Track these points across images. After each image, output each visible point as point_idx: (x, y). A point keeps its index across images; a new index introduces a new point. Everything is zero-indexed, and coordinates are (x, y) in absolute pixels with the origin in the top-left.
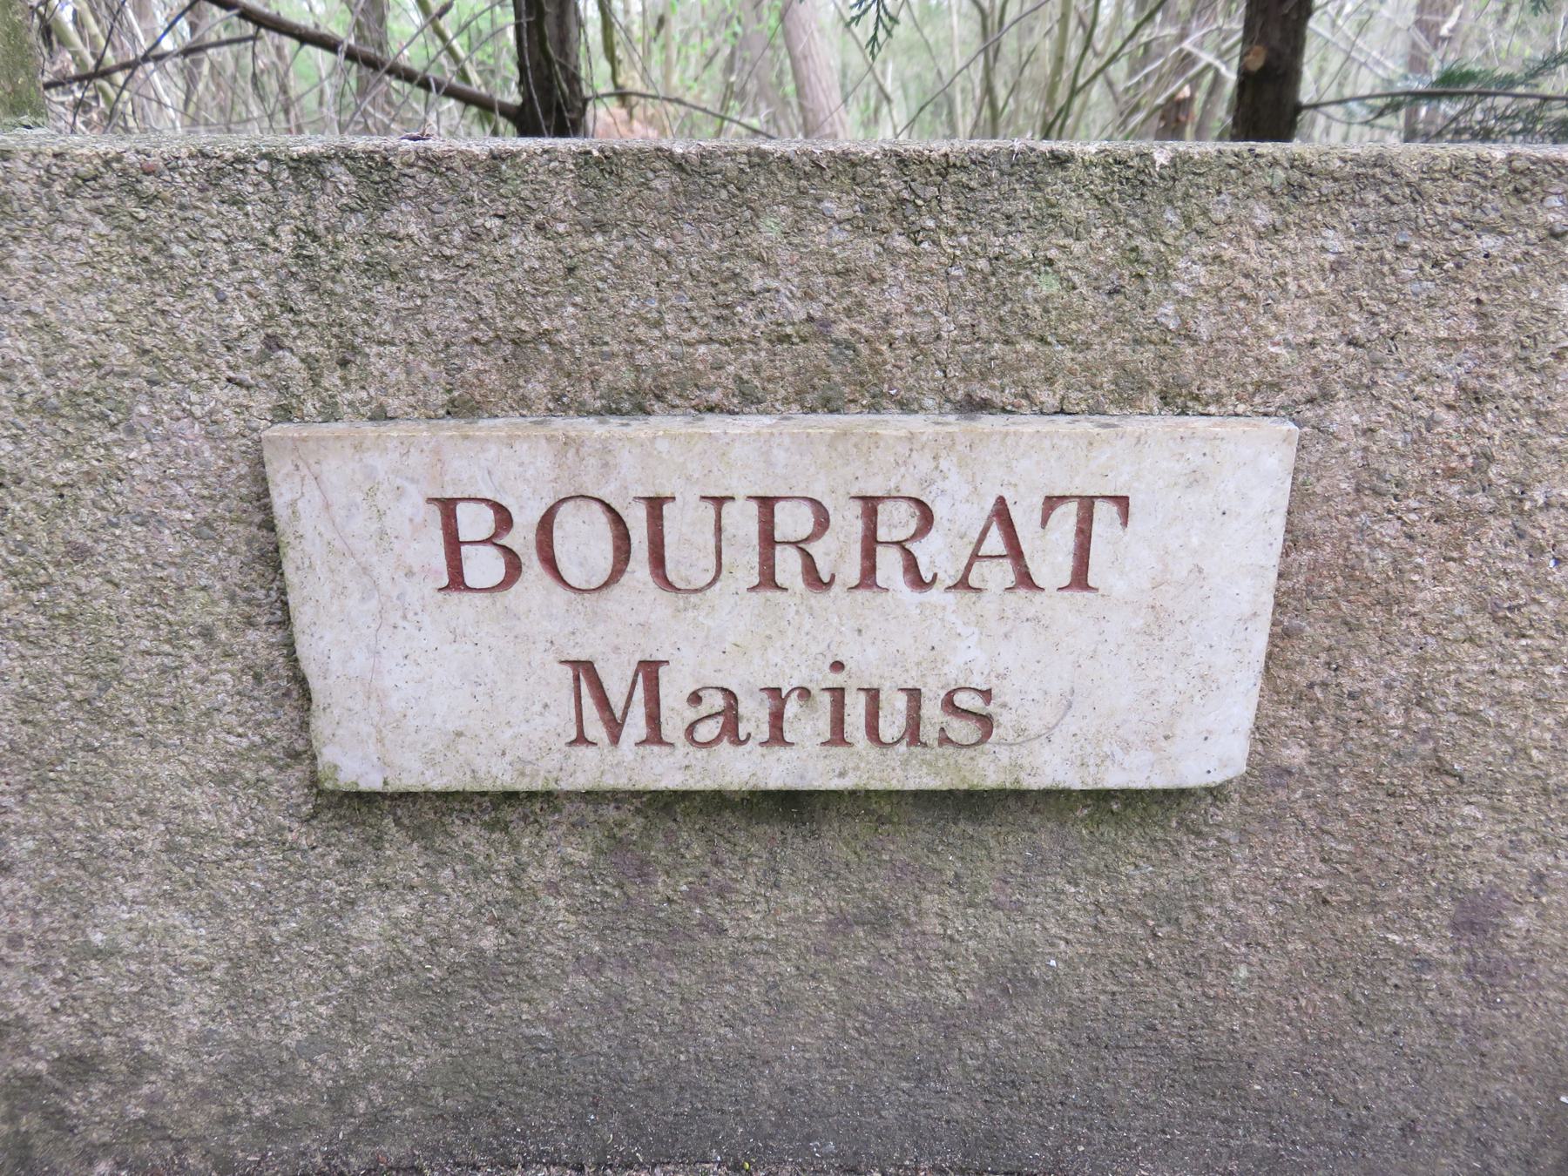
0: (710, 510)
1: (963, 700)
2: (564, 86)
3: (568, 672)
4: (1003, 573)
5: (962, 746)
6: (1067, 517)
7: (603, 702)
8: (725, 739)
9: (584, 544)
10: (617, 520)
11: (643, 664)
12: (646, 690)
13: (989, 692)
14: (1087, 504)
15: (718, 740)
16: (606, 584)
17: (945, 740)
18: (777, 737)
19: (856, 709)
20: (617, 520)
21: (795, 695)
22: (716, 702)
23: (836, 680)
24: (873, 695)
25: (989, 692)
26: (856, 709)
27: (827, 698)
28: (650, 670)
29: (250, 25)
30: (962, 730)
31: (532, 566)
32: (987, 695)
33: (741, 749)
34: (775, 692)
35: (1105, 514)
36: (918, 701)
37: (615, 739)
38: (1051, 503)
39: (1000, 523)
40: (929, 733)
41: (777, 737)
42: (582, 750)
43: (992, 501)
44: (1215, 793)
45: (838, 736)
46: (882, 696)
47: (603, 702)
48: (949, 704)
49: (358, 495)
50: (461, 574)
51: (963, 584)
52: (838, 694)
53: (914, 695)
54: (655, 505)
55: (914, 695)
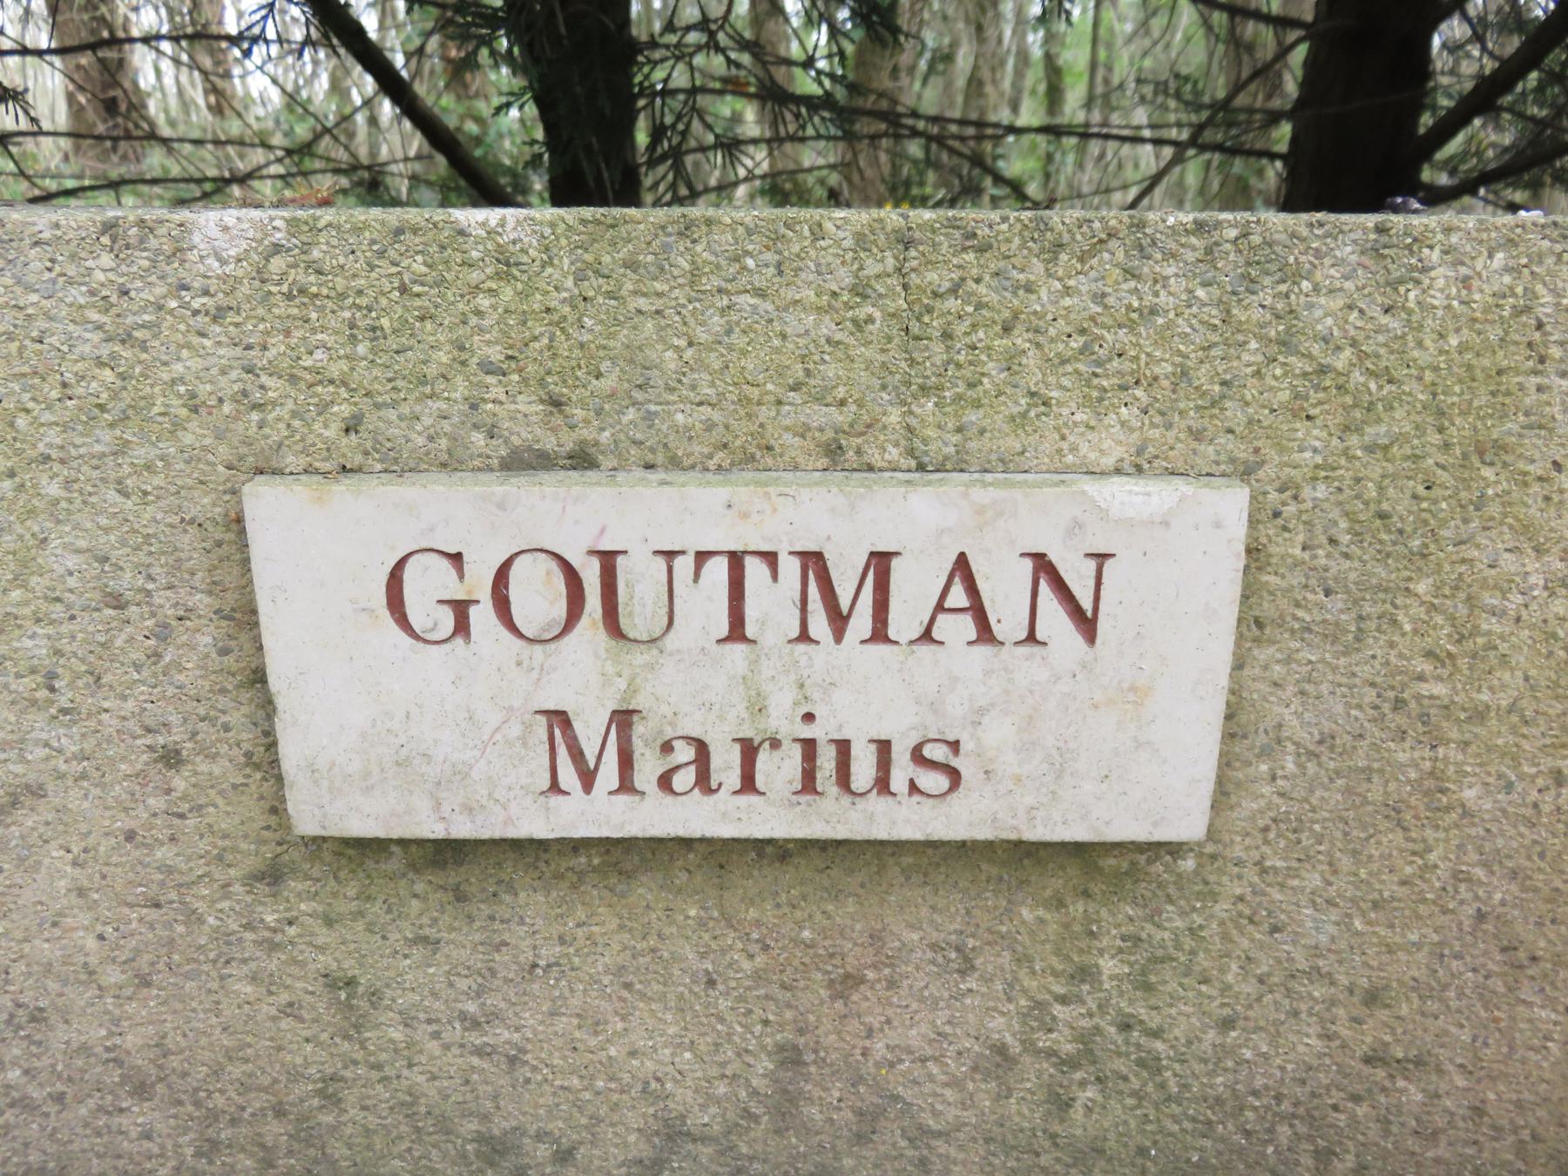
0: (661, 563)
1: (930, 752)
2: (1179, 36)
3: (1028, 564)
4: (965, 626)
5: (929, 796)
6: (718, 570)
7: (577, 755)
8: (696, 790)
9: (537, 596)
10: (572, 577)
11: (872, 554)
12: (619, 737)
13: (957, 743)
14: (736, 561)
15: (869, 791)
16: (556, 637)
17: (913, 788)
18: (748, 783)
19: (827, 761)
20: (572, 577)
21: (766, 745)
22: (684, 753)
23: (807, 732)
24: (843, 747)
25: (957, 743)
26: (827, 761)
27: (797, 752)
28: (881, 562)
29: (369, 79)
30: (933, 781)
31: (483, 616)
32: (955, 746)
33: (715, 797)
34: (709, 791)
35: (755, 570)
36: (889, 751)
37: (839, 635)
38: (702, 557)
39: (1047, 573)
40: (898, 782)
41: (748, 783)
42: (556, 800)
43: (954, 557)
44: (1174, 849)
45: (809, 783)
46: (894, 748)
47: (577, 755)
48: (918, 757)
49: (314, 549)
50: (885, 623)
51: (927, 636)
52: (809, 747)
53: (884, 747)
54: (608, 559)
55: (884, 747)
